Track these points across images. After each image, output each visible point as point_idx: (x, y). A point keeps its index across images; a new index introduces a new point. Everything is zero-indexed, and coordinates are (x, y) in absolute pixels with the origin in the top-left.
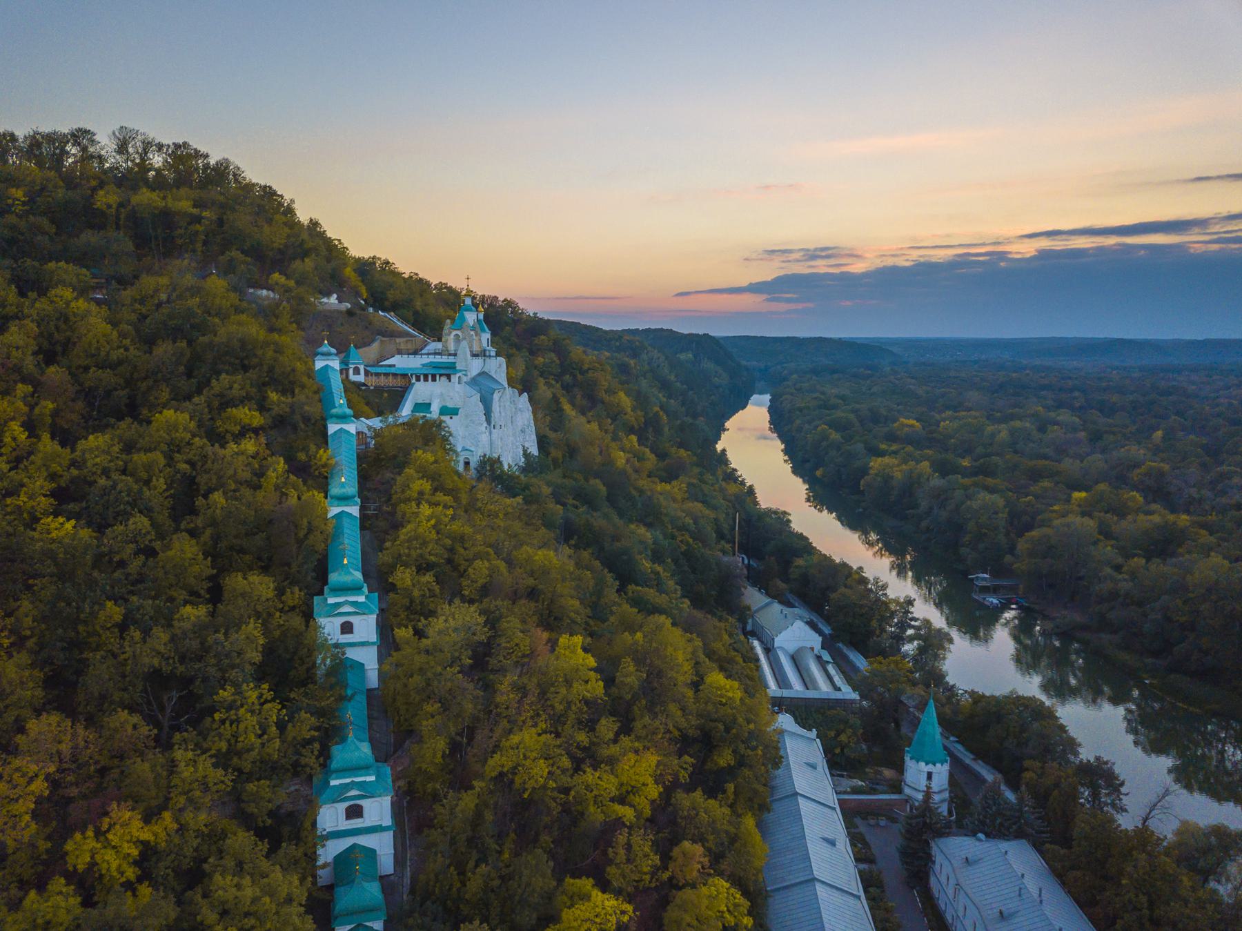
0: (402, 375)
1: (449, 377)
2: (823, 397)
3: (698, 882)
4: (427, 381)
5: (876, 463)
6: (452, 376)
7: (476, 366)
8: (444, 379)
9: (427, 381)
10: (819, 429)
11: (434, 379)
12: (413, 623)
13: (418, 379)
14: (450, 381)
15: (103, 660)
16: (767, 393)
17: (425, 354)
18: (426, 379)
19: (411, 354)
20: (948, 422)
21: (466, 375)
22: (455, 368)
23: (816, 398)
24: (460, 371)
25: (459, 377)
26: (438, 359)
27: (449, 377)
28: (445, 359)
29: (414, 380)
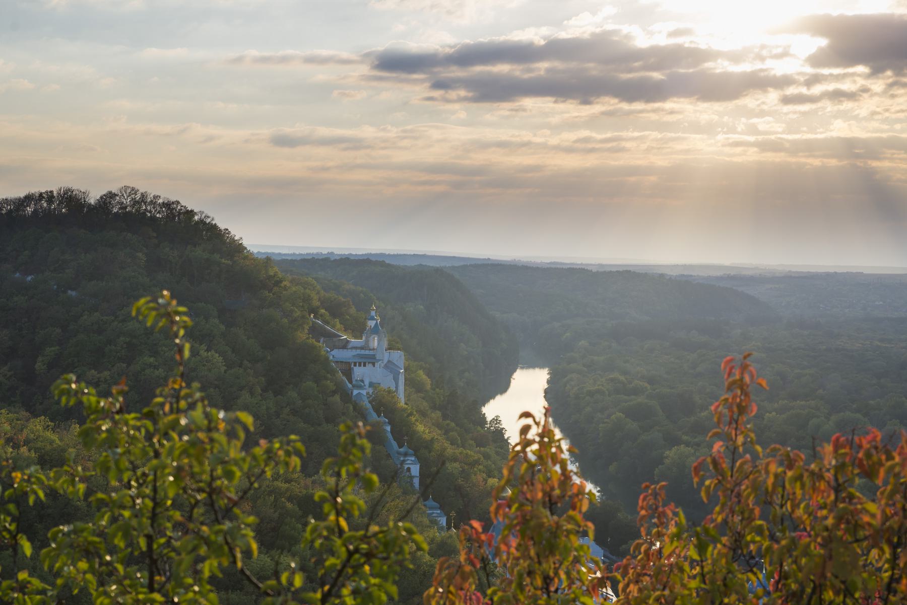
0: (345, 362)
1: (374, 365)
2: (622, 378)
3: (135, 597)
4: (361, 366)
5: (672, 454)
6: (376, 364)
7: (386, 356)
8: (371, 365)
9: (361, 366)
10: (613, 417)
11: (365, 365)
12: (543, 470)
13: (355, 365)
14: (374, 366)
15: (857, 461)
16: (541, 366)
17: (350, 348)
18: (360, 365)
19: (341, 348)
20: (774, 413)
21: (383, 363)
22: (375, 358)
23: (612, 380)
24: (380, 360)
25: (380, 364)
26: (363, 352)
27: (374, 365)
28: (367, 352)
29: (352, 366)
